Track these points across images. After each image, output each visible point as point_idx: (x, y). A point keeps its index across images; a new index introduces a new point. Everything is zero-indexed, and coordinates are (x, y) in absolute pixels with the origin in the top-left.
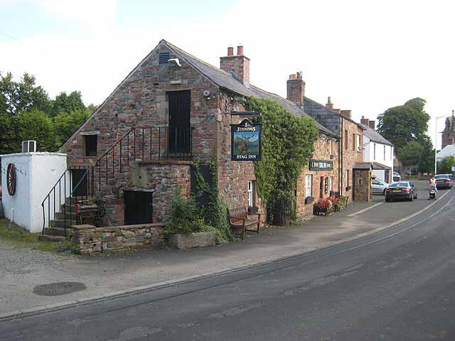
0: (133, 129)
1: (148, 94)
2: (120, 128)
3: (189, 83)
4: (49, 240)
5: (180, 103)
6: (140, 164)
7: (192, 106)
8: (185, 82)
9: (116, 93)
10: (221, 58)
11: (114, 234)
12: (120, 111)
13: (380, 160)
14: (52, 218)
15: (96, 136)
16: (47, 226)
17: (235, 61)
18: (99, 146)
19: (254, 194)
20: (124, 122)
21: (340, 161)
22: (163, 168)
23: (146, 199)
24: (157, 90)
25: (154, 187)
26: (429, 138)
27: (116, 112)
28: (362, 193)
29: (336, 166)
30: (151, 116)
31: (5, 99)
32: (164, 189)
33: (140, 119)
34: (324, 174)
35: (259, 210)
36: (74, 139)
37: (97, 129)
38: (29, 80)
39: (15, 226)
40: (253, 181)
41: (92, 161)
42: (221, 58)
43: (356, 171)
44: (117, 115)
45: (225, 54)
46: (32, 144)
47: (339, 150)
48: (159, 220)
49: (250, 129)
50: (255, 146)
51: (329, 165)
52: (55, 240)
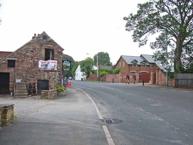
2: (26, 58)
8: (52, 46)
9: (25, 46)
12: (27, 52)
15: (15, 60)
20: (28, 56)
22: (53, 72)
23: (47, 82)
25: (50, 78)
30: (39, 55)
32: (54, 79)
33: (35, 56)
38: (107, 53)
44: (25, 54)
48: (52, 89)
50: (69, 67)
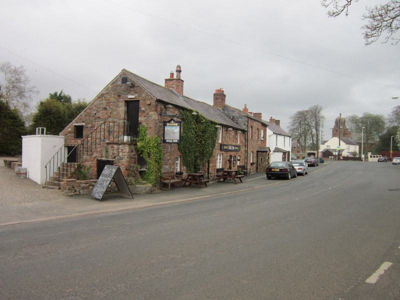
0: (105, 122)
1: (114, 102)
3: (139, 96)
4: (49, 188)
5: (133, 107)
6: (108, 144)
7: (140, 110)
10: (166, 80)
11: (88, 185)
13: (280, 146)
14: (52, 175)
16: (48, 180)
17: (175, 81)
18: (84, 132)
19: (180, 164)
21: (247, 146)
22: (120, 146)
24: (120, 99)
25: (115, 157)
26: (56, 107)
27: (95, 112)
28: (263, 167)
29: (243, 149)
31: (2, 101)
33: (109, 117)
34: (233, 154)
35: (184, 174)
36: (69, 127)
37: (83, 122)
39: (32, 181)
40: (180, 156)
41: (79, 141)
42: (166, 80)
43: (259, 153)
45: (169, 77)
46: (43, 130)
47: (245, 138)
49: (174, 124)
51: (237, 148)
52: (52, 188)
